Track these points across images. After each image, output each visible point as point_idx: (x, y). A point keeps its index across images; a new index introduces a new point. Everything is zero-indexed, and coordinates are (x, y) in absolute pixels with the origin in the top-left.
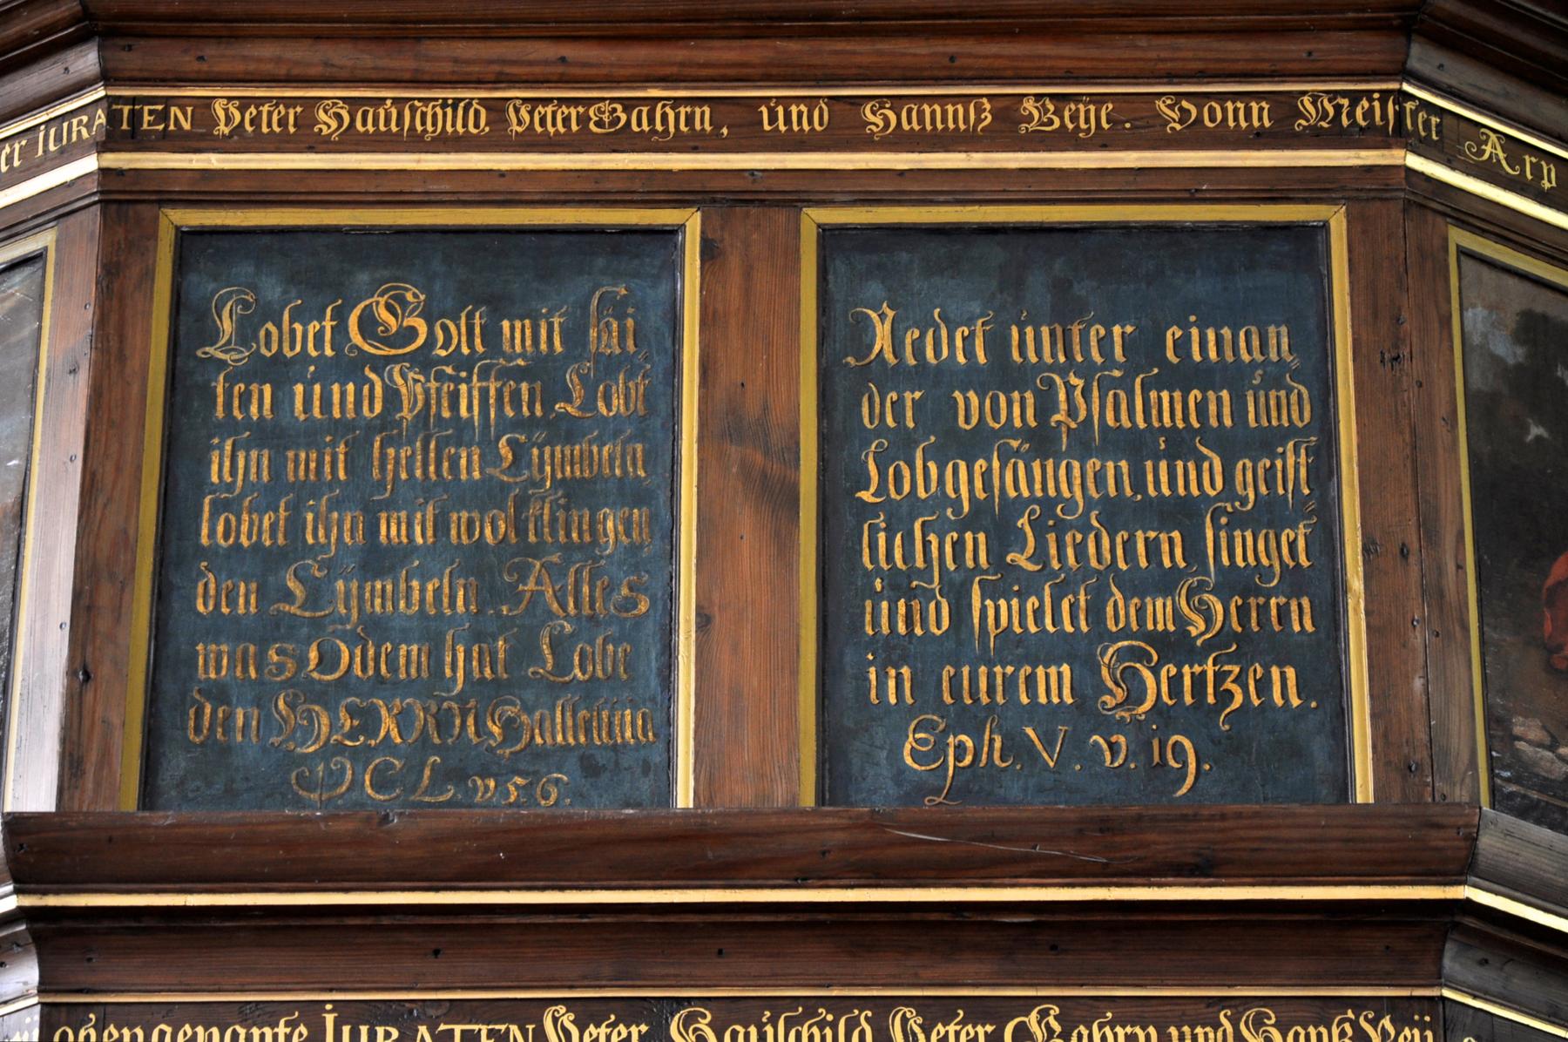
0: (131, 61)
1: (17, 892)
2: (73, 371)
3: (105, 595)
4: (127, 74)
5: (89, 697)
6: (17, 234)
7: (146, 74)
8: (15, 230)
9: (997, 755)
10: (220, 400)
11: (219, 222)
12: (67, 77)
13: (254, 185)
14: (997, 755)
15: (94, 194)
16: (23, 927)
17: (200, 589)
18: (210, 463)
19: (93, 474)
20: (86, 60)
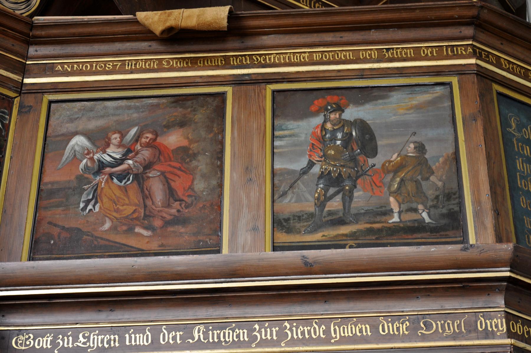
0: (482, 36)
1: (510, 271)
2: (475, 120)
3: (499, 190)
4: (480, 40)
5: (500, 220)
6: (440, 75)
7: (486, 43)
8: (439, 73)
9: (405, 330)
10: (516, 145)
11: (508, 93)
12: (36, 53)
13: (518, 87)
14: (405, 330)
15: (475, 70)
16: (506, 284)
17: (521, 200)
18: (516, 163)
19: (489, 153)
20: (469, 31)
